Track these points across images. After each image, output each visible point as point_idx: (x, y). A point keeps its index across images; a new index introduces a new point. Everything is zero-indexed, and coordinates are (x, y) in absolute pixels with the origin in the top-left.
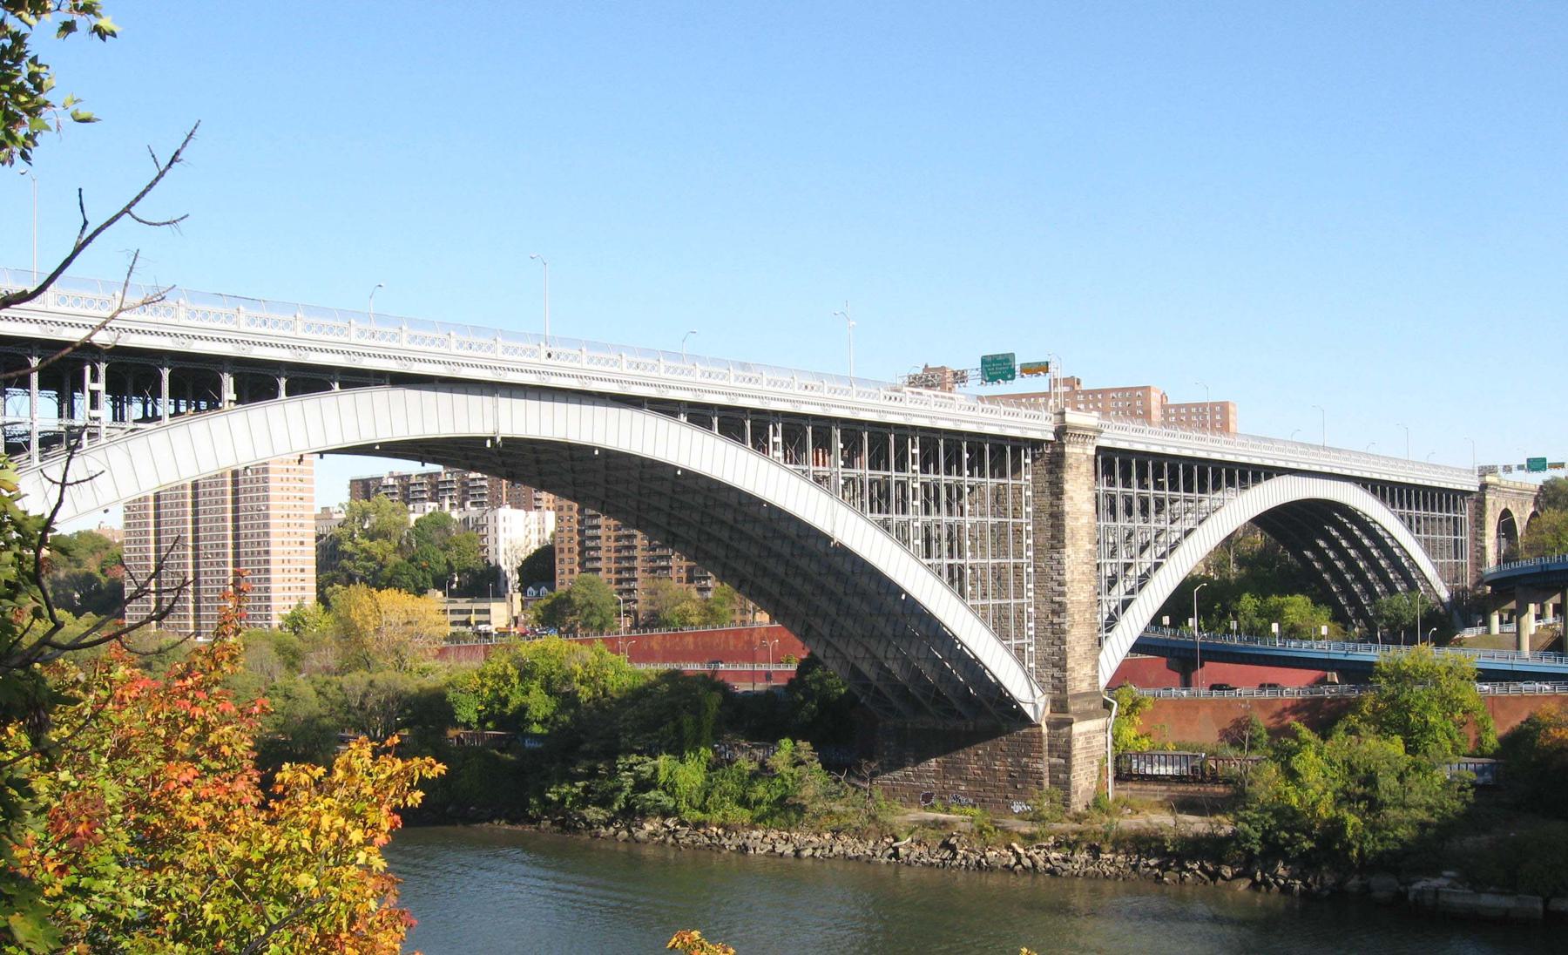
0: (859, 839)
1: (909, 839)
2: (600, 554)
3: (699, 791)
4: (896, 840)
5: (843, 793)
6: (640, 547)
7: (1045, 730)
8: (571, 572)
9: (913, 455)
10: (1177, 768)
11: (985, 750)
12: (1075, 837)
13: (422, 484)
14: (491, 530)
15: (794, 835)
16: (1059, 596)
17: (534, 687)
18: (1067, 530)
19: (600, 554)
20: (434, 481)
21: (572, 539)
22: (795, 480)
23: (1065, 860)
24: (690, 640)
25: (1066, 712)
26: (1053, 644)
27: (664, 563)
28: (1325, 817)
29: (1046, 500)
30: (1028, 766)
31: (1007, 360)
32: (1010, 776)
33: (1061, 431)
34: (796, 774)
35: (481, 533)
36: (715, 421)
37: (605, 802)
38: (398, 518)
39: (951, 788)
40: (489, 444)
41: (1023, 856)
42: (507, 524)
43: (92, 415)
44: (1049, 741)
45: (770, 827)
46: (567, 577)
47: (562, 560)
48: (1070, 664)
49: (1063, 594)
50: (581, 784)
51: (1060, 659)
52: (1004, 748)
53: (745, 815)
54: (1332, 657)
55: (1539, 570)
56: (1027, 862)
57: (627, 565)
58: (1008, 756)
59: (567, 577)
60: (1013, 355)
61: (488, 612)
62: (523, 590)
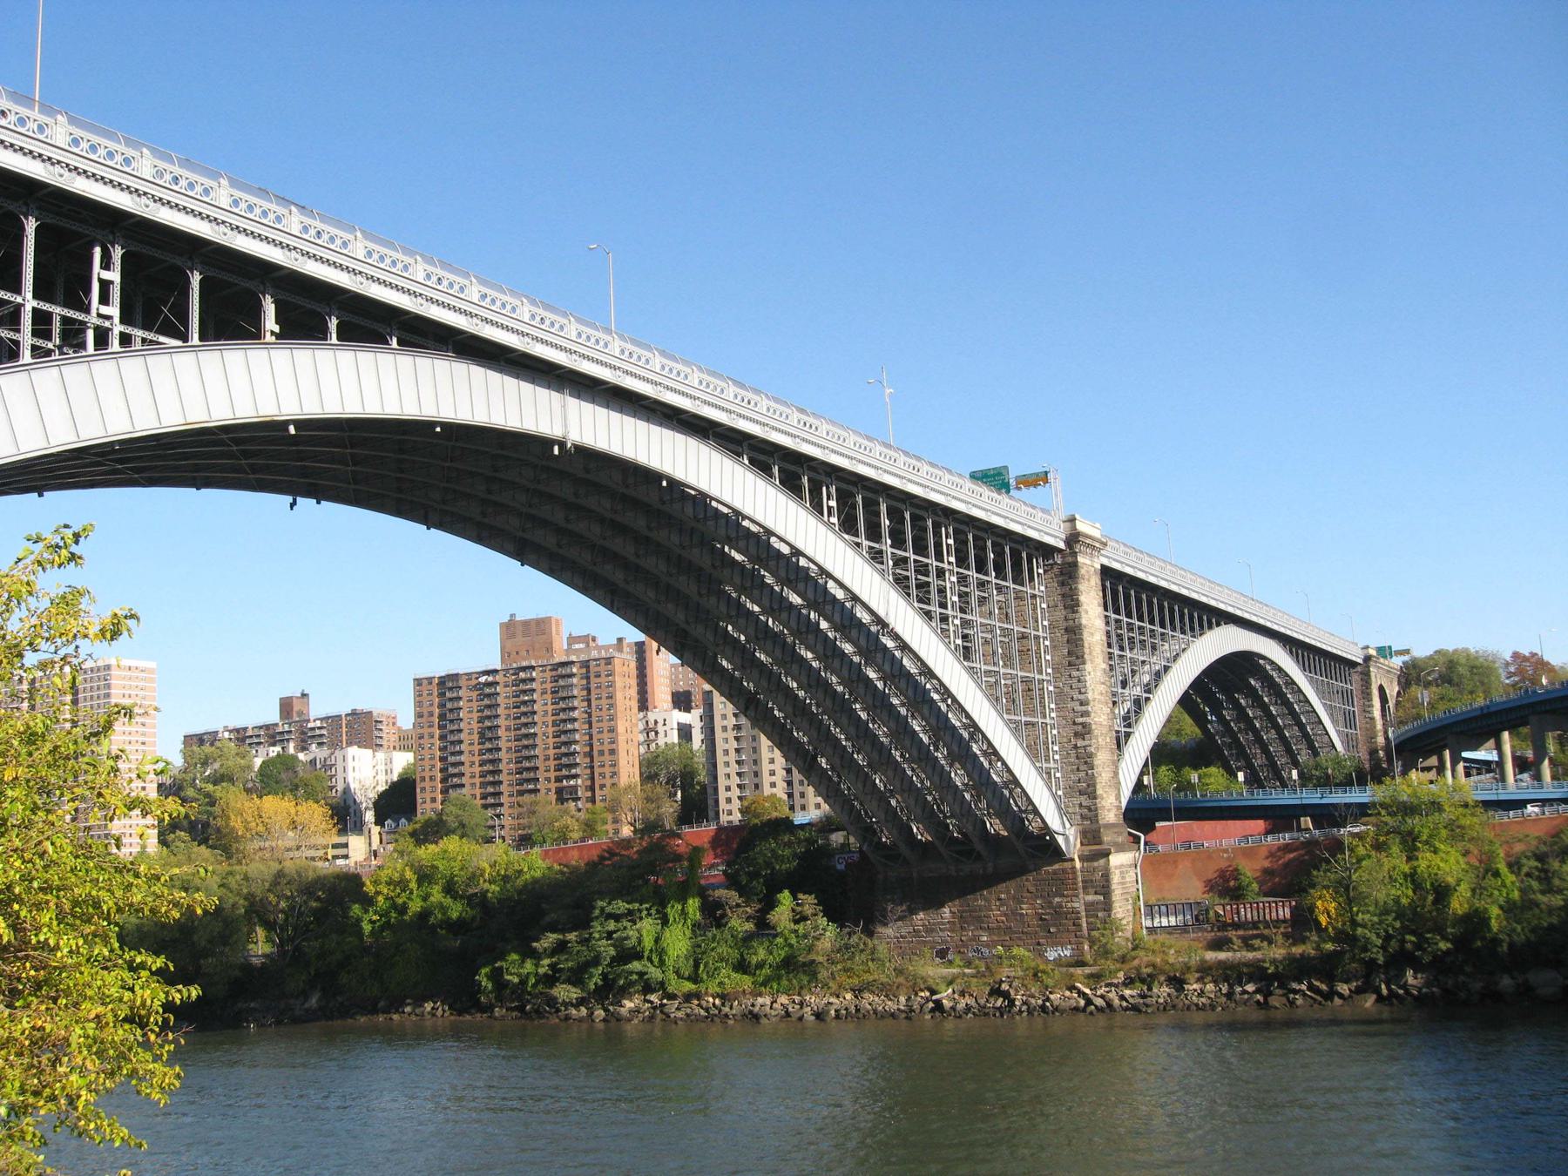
0: (887, 996)
1: (950, 990)
2: (464, 780)
3: (687, 959)
4: (933, 992)
5: (862, 946)
6: (505, 772)
7: (1078, 864)
8: (434, 800)
9: (948, 545)
10: (1180, 917)
11: (1008, 892)
12: (1149, 970)
13: (259, 736)
14: (340, 770)
15: (808, 998)
16: (1082, 716)
17: (434, 892)
18: (1086, 645)
19: (464, 780)
20: (271, 732)
21: (433, 766)
22: (850, 552)
23: (1143, 996)
24: (575, 854)
25: (1100, 843)
26: (1078, 770)
27: (531, 787)
28: (1460, 912)
29: (1060, 613)
30: (1061, 907)
31: (1000, 474)
32: (1041, 919)
33: (1074, 538)
34: (801, 931)
35: (329, 773)
36: (776, 470)
37: (576, 978)
38: (242, 761)
39: (971, 940)
40: (556, 451)
41: (1092, 997)
42: (356, 764)
43: (101, 312)
44: (1083, 876)
45: (778, 991)
46: (428, 806)
47: (423, 789)
48: (1099, 791)
49: (1086, 714)
50: (546, 962)
51: (1088, 785)
52: (1032, 889)
53: (746, 982)
54: (1305, 801)
55: (1479, 713)
56: (1099, 1002)
57: (492, 790)
58: (1037, 897)
59: (428, 806)
60: (1006, 468)
61: (346, 845)
62: (379, 821)
